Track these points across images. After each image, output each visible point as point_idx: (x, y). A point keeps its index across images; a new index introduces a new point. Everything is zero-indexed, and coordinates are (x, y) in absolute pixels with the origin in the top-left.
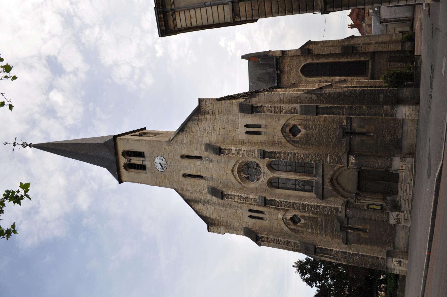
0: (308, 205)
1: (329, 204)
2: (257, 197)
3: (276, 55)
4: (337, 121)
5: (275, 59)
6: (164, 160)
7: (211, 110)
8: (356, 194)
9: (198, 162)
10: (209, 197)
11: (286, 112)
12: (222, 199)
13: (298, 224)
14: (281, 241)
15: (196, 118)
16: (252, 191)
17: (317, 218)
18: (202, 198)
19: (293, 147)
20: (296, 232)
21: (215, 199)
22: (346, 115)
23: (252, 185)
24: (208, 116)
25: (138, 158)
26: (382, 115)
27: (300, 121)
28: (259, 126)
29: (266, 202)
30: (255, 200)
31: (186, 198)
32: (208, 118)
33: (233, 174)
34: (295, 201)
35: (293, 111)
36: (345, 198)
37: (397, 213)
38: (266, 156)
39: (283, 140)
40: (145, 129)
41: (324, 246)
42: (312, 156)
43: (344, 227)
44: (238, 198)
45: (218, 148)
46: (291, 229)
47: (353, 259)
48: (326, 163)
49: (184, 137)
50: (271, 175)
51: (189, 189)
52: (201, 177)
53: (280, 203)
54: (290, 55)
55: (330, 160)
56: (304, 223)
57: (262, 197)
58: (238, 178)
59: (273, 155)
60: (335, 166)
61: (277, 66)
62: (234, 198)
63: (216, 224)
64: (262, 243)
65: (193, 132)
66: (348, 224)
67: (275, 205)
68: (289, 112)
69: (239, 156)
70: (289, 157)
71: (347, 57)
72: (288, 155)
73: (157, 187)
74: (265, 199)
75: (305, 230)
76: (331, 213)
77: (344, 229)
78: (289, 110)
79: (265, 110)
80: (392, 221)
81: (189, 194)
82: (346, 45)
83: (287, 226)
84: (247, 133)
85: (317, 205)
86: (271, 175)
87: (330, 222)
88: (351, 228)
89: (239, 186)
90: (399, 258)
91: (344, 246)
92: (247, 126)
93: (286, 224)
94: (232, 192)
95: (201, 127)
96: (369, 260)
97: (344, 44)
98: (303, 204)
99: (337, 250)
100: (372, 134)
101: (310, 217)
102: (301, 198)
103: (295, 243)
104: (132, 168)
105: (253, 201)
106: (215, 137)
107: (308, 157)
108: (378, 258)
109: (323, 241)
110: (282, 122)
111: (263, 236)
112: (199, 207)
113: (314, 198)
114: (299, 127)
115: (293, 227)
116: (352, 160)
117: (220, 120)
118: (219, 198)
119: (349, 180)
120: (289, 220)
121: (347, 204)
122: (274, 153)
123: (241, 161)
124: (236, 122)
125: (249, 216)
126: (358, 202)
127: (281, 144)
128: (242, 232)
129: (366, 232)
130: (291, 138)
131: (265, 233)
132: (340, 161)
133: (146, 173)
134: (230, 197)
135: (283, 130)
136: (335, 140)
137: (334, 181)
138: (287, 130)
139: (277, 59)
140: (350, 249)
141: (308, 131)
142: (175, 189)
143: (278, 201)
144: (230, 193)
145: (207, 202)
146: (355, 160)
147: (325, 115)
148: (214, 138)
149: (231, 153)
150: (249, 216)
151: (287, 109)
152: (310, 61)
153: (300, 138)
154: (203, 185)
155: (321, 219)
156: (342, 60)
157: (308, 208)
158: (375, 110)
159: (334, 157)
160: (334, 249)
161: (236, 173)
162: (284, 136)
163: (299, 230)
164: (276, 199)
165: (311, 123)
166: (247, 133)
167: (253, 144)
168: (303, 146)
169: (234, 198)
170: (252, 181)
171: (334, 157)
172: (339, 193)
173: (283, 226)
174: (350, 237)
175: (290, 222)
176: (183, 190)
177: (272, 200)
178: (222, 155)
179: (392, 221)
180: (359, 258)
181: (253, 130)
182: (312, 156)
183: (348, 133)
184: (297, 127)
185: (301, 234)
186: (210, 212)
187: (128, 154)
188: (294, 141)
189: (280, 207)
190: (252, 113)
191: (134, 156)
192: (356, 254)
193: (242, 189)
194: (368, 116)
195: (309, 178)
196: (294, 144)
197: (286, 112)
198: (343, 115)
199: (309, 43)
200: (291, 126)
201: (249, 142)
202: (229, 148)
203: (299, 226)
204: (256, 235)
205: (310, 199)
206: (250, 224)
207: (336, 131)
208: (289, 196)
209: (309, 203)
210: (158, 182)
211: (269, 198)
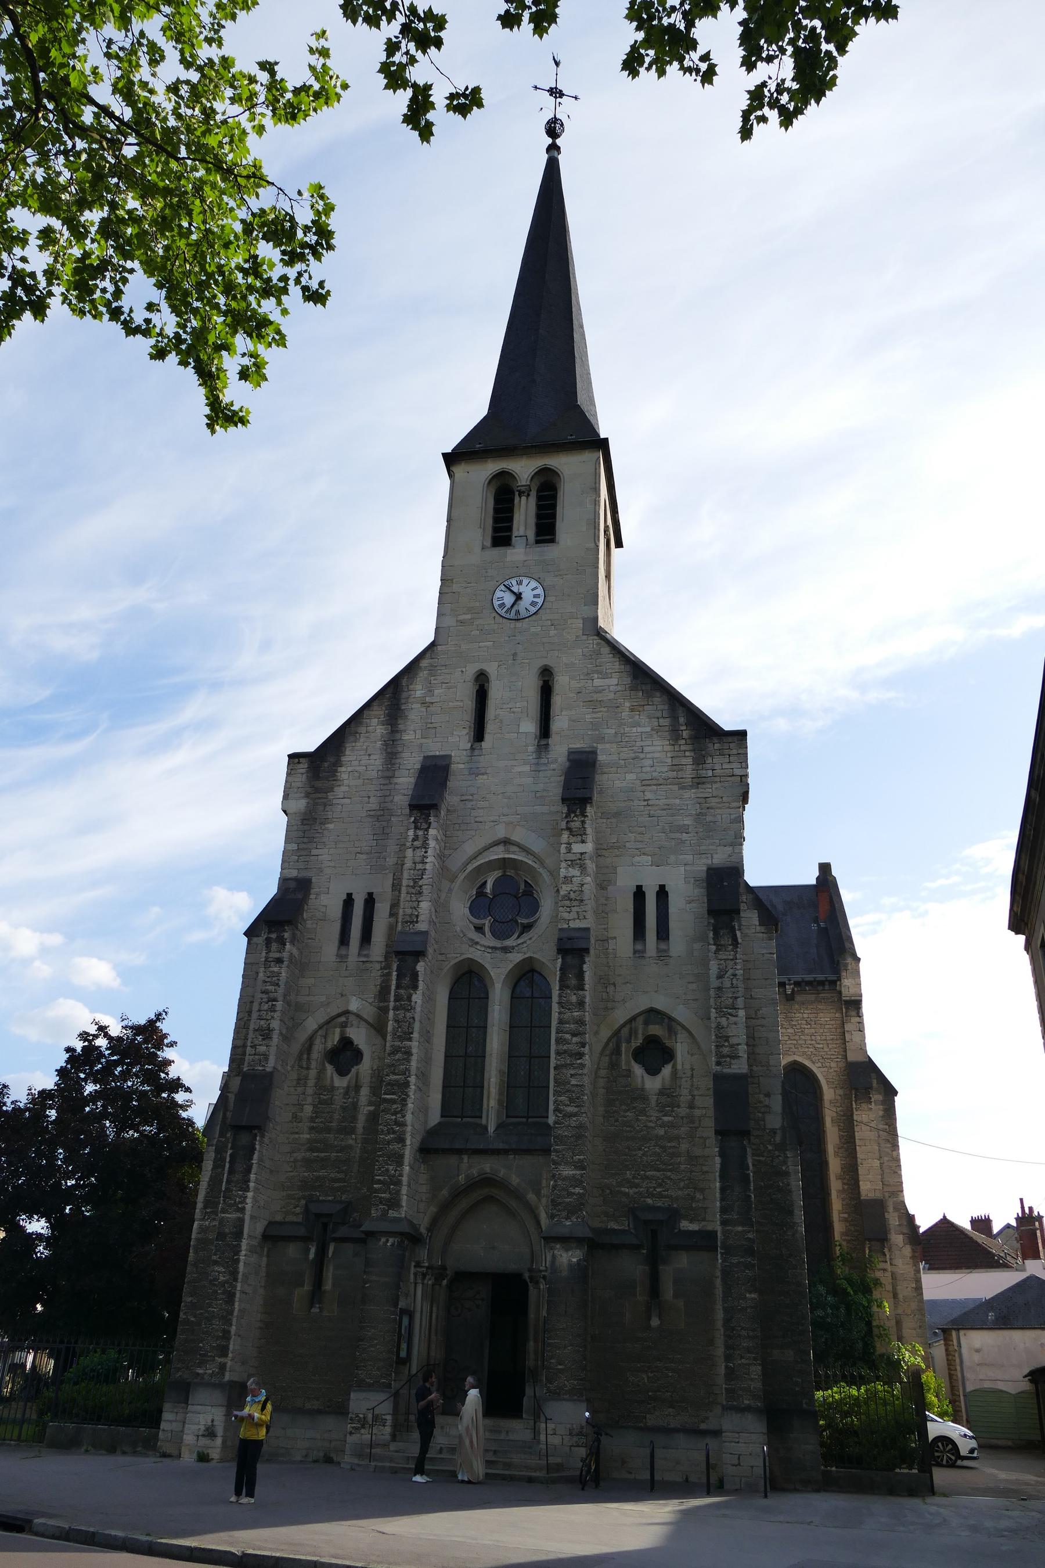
0: (404, 1102)
1: (409, 1176)
2: (422, 926)
3: (847, 982)
4: (693, 1199)
5: (833, 977)
6: (533, 610)
7: (710, 773)
8: (444, 1268)
9: (530, 727)
10: (411, 762)
11: (719, 1027)
12: (413, 807)
13: (330, 1069)
14: (272, 1009)
15: (682, 720)
16: (440, 907)
17: (353, 1131)
18: (406, 737)
19: (598, 1048)
20: (300, 1058)
21: (406, 780)
22: (724, 1232)
23: (460, 909)
24: (690, 761)
25: (532, 520)
26: (728, 1358)
27: (689, 1073)
28: (663, 933)
29: (406, 955)
30: (414, 920)
31: (404, 682)
32: (684, 761)
33: (496, 843)
34: (414, 1059)
35: (726, 1050)
36: (429, 1230)
37: (389, 1417)
38: (569, 959)
39: (621, 1016)
40: (619, 544)
41: (260, 1160)
42: (575, 1115)
43: (325, 1226)
44: (418, 859)
45: (588, 795)
46: (311, 1039)
47: (216, 1263)
48: (555, 1163)
49: (612, 681)
50: (499, 973)
51: (436, 692)
52: (479, 734)
53: (404, 1004)
54: (847, 1027)
55: (564, 1179)
56: (333, 1089)
57: (425, 943)
58: (481, 861)
59: (573, 982)
60: (538, 1194)
61: (809, 983)
62: (415, 848)
63: (318, 784)
64: (260, 940)
65: (632, 710)
66: (335, 1240)
67: (398, 987)
68: (723, 1038)
69: (563, 865)
70: (568, 1036)
71: (845, 1220)
72: (574, 1035)
73: (439, 583)
74: (419, 954)
75: (310, 1091)
76: (379, 1182)
77: (324, 1226)
78: (727, 1038)
79: (722, 955)
80: (360, 1402)
81: (419, 694)
82: (887, 1216)
83: (320, 1027)
84: (639, 894)
85: (404, 1133)
86: (499, 973)
87: (341, 1176)
88: (322, 1252)
89: (456, 862)
90: (226, 1430)
91: (260, 1227)
92: (662, 893)
93: (328, 1022)
94: (437, 840)
95: (651, 736)
96: (216, 1322)
97: (891, 1209)
98: (407, 1084)
99: (248, 1207)
100: (655, 1322)
101: (355, 1106)
102: (424, 1077)
103: (266, 1057)
104: (497, 500)
105: (409, 911)
106: (618, 784)
107: (571, 1100)
108: (224, 1351)
109: (277, 1152)
110: (681, 1013)
111: (288, 946)
112: (376, 728)
113: (426, 1122)
114: (667, 1070)
115: (318, 1047)
116: (568, 1257)
117: (677, 801)
118: (413, 797)
119: (489, 1244)
120: (342, 1033)
121: (412, 1238)
122: (581, 987)
123: (541, 870)
124: (672, 858)
125: (350, 895)
126: (415, 1274)
127: (606, 1009)
128: (294, 873)
129: (312, 1306)
130: (629, 1041)
131: (295, 952)
132: (564, 1214)
133: (483, 548)
134: (420, 833)
135: (653, 1014)
136: (627, 1195)
137: (487, 1192)
138: (655, 1030)
139: (834, 984)
140: (251, 1250)
141: (653, 1100)
142: (432, 645)
143: (414, 998)
144: (432, 832)
145: (391, 752)
146: (570, 1265)
147: (718, 1160)
148: (614, 781)
149: (572, 839)
150: (350, 895)
151: (732, 1031)
152: (829, 1093)
153: (629, 1073)
154: (454, 742)
155: (350, 1147)
156: (837, 1205)
157: (393, 1101)
158: (744, 1333)
159: (577, 1190)
160: (250, 1194)
161: (498, 853)
162: (633, 1019)
163: (308, 1068)
164: (419, 992)
165: (683, 1111)
166: (639, 894)
167: (603, 913)
168: (601, 1082)
169: (415, 848)
170: (471, 909)
171: (577, 1190)
172: (445, 1207)
173: (321, 1016)
174: (292, 1251)
175: (337, 1038)
176: (433, 670)
177: (415, 976)
178: (565, 810)
179: (360, 1402)
180: (223, 1284)
181: (649, 911)
182: (575, 1115)
183: (656, 1235)
184: (667, 1062)
185: (294, 1076)
186: (361, 762)
187: (548, 489)
188: (617, 1051)
189: (392, 1004)
190: (711, 912)
191: (539, 507)
192: (234, 1274)
193: (444, 872)
194: (725, 1310)
195: (493, 1103)
196: (608, 1052)
197: (719, 1027)
198: (724, 1223)
199: (890, 1092)
200: (668, 1043)
201: (607, 899)
202: (589, 831)
203: (322, 1071)
204: (289, 922)
205: (423, 1106)
206: (324, 899)
207: (660, 1196)
208: (427, 1037)
209: (410, 1106)
210: (455, 587)
211: (420, 967)
